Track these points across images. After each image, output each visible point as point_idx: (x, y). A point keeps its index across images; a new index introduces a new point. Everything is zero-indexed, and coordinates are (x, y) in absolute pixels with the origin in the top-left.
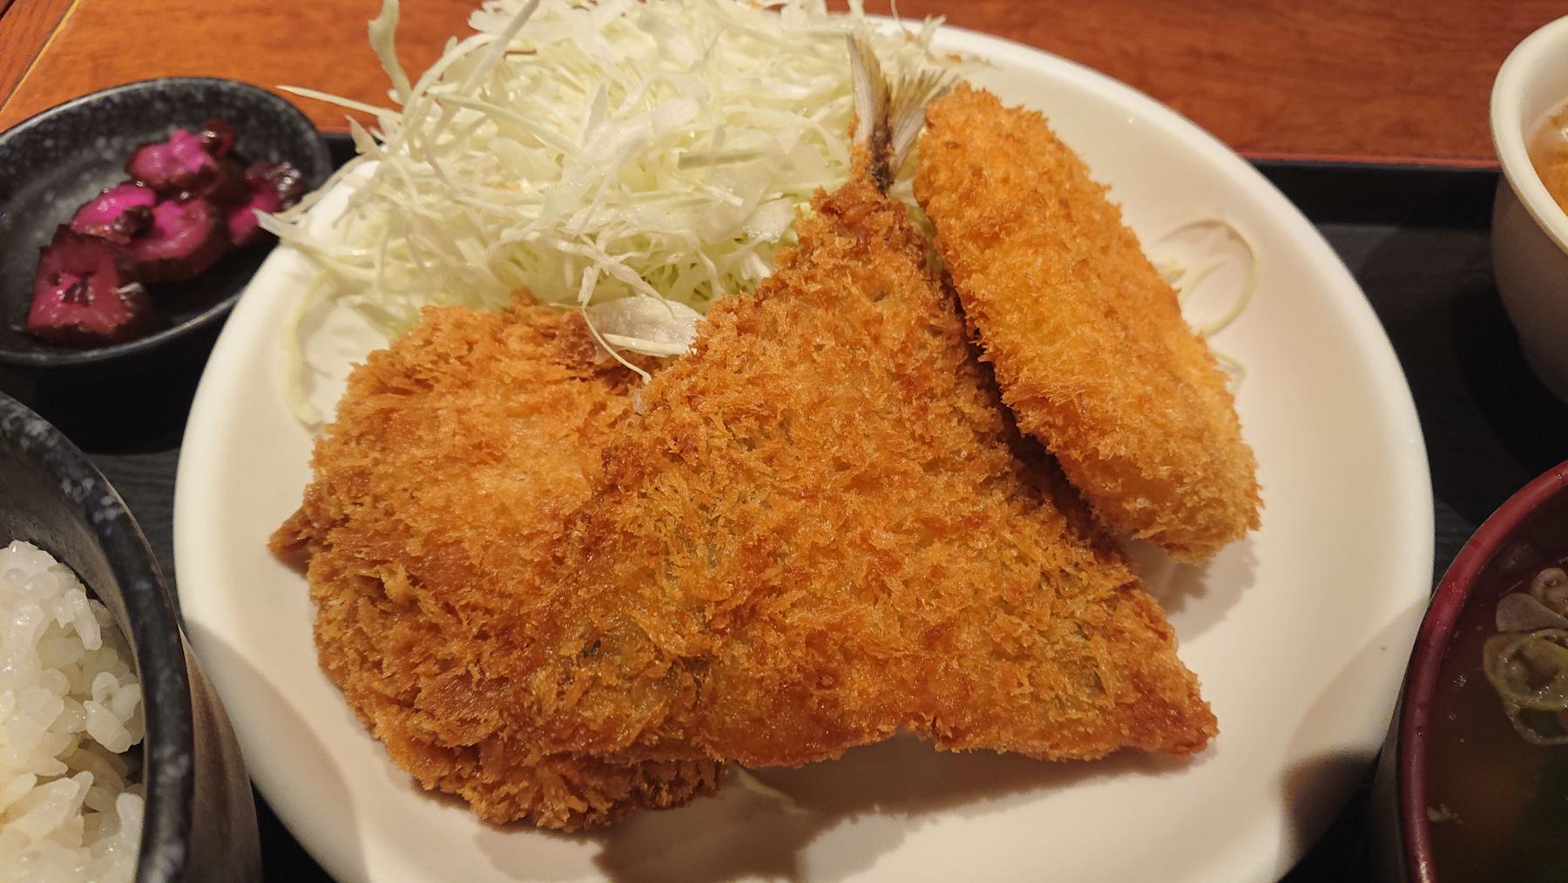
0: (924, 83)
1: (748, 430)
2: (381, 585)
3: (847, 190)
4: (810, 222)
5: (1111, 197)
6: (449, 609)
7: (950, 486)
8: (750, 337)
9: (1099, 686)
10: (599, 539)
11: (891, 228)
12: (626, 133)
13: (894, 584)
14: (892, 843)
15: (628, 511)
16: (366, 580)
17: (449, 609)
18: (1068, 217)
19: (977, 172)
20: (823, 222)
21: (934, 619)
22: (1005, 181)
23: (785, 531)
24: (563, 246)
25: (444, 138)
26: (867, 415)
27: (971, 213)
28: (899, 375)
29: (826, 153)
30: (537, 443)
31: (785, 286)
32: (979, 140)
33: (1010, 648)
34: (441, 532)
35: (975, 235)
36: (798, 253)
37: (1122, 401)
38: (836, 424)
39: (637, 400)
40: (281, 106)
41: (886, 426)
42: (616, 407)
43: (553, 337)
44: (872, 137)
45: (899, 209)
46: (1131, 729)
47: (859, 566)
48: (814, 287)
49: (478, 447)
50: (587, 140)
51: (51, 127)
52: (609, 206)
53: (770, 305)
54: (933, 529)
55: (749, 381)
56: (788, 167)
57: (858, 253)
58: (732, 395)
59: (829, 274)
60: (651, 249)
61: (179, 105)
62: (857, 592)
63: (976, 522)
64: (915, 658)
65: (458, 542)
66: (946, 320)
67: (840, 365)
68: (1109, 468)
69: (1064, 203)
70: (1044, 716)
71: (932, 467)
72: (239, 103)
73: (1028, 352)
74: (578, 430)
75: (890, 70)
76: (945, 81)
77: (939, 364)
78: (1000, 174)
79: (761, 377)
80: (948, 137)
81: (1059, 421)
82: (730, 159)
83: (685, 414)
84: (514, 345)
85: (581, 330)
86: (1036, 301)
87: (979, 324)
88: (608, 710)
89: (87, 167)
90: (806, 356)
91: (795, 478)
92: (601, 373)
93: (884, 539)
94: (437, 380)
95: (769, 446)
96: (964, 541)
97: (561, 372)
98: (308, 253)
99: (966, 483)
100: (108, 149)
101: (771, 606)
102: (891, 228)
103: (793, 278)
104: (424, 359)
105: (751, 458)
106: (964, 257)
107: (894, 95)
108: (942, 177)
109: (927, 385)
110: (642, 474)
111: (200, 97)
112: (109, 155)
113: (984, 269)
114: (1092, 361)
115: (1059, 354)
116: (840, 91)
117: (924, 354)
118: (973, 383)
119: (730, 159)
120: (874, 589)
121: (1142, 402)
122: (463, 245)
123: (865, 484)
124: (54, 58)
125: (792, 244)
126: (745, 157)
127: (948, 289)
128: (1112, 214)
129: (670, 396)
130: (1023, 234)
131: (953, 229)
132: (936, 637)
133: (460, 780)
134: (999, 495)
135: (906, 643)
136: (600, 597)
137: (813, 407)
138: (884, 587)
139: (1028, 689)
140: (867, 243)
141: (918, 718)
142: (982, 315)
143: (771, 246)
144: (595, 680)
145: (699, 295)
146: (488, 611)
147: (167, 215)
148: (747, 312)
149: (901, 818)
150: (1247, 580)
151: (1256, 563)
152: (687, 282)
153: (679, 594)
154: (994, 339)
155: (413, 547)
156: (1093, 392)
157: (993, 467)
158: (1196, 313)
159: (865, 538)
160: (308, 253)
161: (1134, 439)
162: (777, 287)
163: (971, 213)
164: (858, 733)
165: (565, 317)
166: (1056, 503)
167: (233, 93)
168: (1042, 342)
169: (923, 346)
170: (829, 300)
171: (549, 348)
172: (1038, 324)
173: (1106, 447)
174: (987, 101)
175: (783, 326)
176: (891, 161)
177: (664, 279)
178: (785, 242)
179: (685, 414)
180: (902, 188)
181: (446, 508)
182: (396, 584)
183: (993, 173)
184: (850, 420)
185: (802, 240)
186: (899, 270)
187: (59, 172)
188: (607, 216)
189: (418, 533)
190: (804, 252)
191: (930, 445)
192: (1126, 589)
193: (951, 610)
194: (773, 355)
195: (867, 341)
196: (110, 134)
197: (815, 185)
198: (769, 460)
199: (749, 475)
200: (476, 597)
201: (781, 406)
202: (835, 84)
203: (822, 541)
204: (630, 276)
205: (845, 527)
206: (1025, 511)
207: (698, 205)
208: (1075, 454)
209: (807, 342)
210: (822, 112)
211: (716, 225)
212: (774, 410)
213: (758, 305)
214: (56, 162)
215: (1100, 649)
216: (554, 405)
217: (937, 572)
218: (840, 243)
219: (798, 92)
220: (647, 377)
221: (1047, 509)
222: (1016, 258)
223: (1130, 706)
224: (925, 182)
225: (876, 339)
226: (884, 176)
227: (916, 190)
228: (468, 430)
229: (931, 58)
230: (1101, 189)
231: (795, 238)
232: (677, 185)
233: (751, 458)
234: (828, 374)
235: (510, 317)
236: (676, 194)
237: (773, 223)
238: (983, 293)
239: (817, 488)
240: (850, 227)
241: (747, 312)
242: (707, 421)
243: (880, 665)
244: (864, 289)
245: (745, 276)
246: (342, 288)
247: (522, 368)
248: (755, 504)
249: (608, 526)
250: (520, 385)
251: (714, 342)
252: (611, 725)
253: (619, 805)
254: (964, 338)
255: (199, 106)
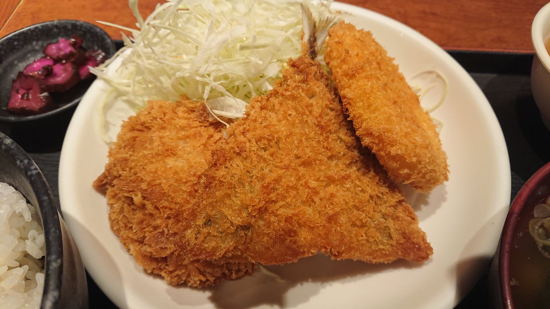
0: (328, 21)
1: (264, 144)
2: (132, 199)
3: (300, 59)
4: (287, 70)
5: (395, 62)
6: (157, 208)
7: (337, 165)
8: (265, 111)
9: (390, 237)
10: (210, 183)
11: (316, 72)
12: (220, 38)
13: (317, 199)
14: (315, 292)
15: (221, 173)
16: (127, 197)
17: (157, 208)
18: (380, 68)
19: (347, 52)
20: (291, 70)
21: (331, 212)
22: (357, 55)
23: (277, 181)
24: (198, 78)
25: (156, 40)
26: (307, 139)
27: (345, 67)
28: (319, 125)
29: (293, 46)
30: (188, 149)
31: (278, 93)
32: (348, 41)
33: (358, 223)
34: (154, 180)
35: (346, 75)
36: (282, 81)
37: (399, 134)
38: (296, 142)
39: (224, 134)
40: (98, 30)
41: (314, 143)
42: (217, 136)
43: (194, 111)
44: (309, 40)
45: (319, 65)
46: (402, 252)
47: (304, 193)
48: (288, 93)
49: (167, 150)
50: (207, 40)
51: (17, 37)
52: (215, 64)
53: (272, 99)
54: (331, 180)
55: (265, 127)
56: (279, 50)
57: (304, 81)
58: (258, 132)
59: (293, 88)
60: (230, 80)
61: (62, 30)
62: (303, 202)
63: (346, 178)
64: (324, 226)
65: (160, 184)
66: (336, 105)
67: (297, 121)
68: (395, 158)
69: (378, 64)
70: (370, 247)
71: (330, 158)
72: (83, 29)
73: (365, 117)
74: (203, 144)
75: (316, 16)
76: (336, 20)
77: (333, 121)
78: (355, 53)
79: (269, 125)
80: (337, 40)
81: (377, 141)
82: (258, 47)
83: (241, 138)
84: (180, 114)
85: (204, 109)
86: (368, 98)
87: (348, 106)
88: (213, 244)
89: (29, 52)
90: (285, 118)
91: (281, 162)
92: (211, 124)
93: (313, 184)
94: (153, 126)
95: (272, 150)
96: (342, 184)
97: (197, 124)
98: (107, 81)
99: (343, 164)
100: (36, 45)
101: (272, 207)
102: (316, 72)
103: (281, 90)
104: (148, 119)
105: (265, 155)
106: (342, 83)
107: (317, 25)
108: (335, 54)
109: (328, 129)
110: (226, 160)
111: (70, 27)
112: (37, 47)
113: (349, 87)
114: (388, 120)
115: (376, 117)
116: (298, 24)
117: (328, 118)
118: (345, 128)
119: (258, 47)
120: (310, 202)
121: (407, 134)
122: (162, 79)
123: (306, 164)
124: (18, 14)
125: (281, 78)
126: (263, 46)
127: (337, 94)
128: (395, 68)
129: (236, 132)
130: (364, 74)
131: (339, 72)
132: (332, 219)
133: (160, 269)
134: (355, 168)
135: (321, 221)
136: (211, 204)
137: (288, 136)
138: (313, 201)
139: (365, 238)
140: (307, 78)
141: (326, 248)
142: (349, 103)
143: (272, 79)
144: (209, 233)
145: (247, 97)
146: (171, 209)
147: (57, 69)
148: (264, 102)
149: (319, 284)
150: (444, 199)
151: (446, 193)
152: (243, 91)
153: (239, 203)
154: (353, 112)
155: (144, 186)
156: (388, 131)
157: (352, 158)
158: (425, 104)
159: (306, 183)
160: (107, 81)
161: (403, 148)
162: (275, 93)
163: (345, 67)
164: (304, 253)
165: (199, 104)
166: (375, 171)
167: (81, 26)
168: (370, 113)
169: (327, 115)
170: (293, 98)
171: (193, 115)
172: (369, 106)
173: (393, 151)
174: (351, 27)
175: (277, 107)
176: (316, 48)
177: (234, 91)
178: (277, 77)
179: (241, 138)
180: (320, 58)
181: (156, 172)
182: (137, 199)
183: (353, 52)
184: (301, 141)
185: (284, 77)
186: (319, 87)
187: (20, 53)
188: (213, 68)
189: (146, 181)
190: (285, 81)
191: (330, 150)
192: (400, 202)
193: (337, 209)
194: (273, 117)
195: (307, 113)
196: (38, 40)
197: (289, 57)
198: (272, 155)
199: (265, 160)
200: (166, 204)
201: (276, 136)
202: (296, 21)
203: (291, 184)
204: (222, 89)
205: (299, 179)
206: (364, 174)
207: (247, 63)
208: (382, 153)
209: (286, 113)
210: (291, 31)
211: (253, 71)
212: (273, 137)
213: (268, 100)
214: (18, 50)
215: (391, 223)
216: (194, 135)
217: (332, 195)
218: (298, 77)
219: (283, 24)
220: (228, 125)
221: (372, 173)
222: (361, 83)
223: (402, 244)
224: (328, 56)
225: (310, 112)
226: (313, 54)
227: (325, 59)
228: (164, 144)
229: (330, 12)
230: (391, 60)
231: (281, 76)
232: (240, 56)
233: (265, 155)
234: (293, 124)
235: (179, 104)
236: (238, 60)
237: (273, 71)
238: (349, 95)
239: (289, 165)
240: (301, 72)
241: (264, 102)
242: (250, 141)
243: (311, 229)
244: (306, 94)
245: (263, 90)
246: (119, 94)
247: (183, 122)
248: (266, 171)
249: (213, 178)
250: (183, 128)
251: (252, 112)
252: (215, 249)
253: (217, 278)
254: (342, 112)
255: (69, 30)
